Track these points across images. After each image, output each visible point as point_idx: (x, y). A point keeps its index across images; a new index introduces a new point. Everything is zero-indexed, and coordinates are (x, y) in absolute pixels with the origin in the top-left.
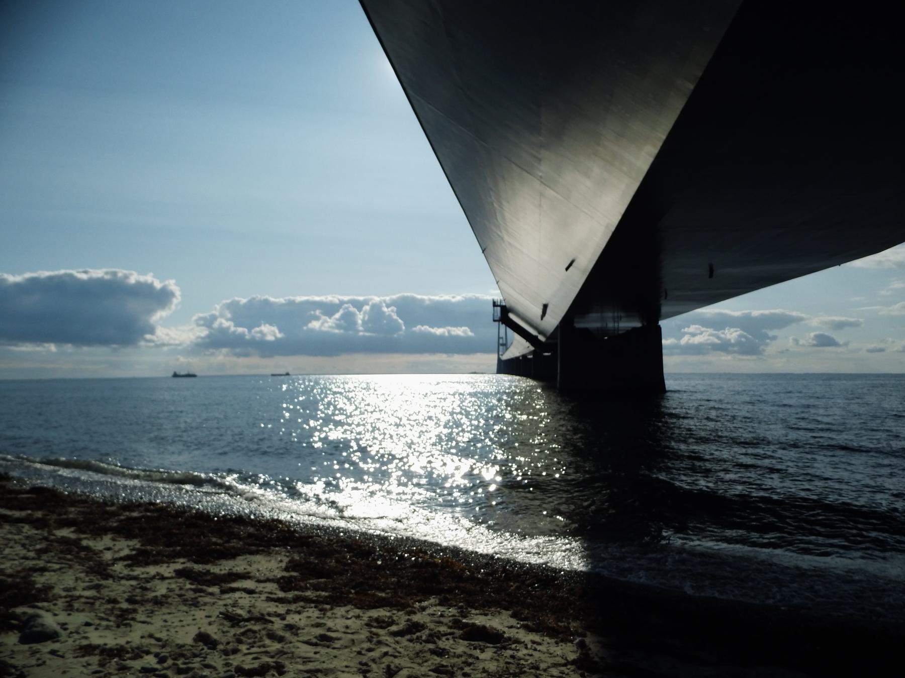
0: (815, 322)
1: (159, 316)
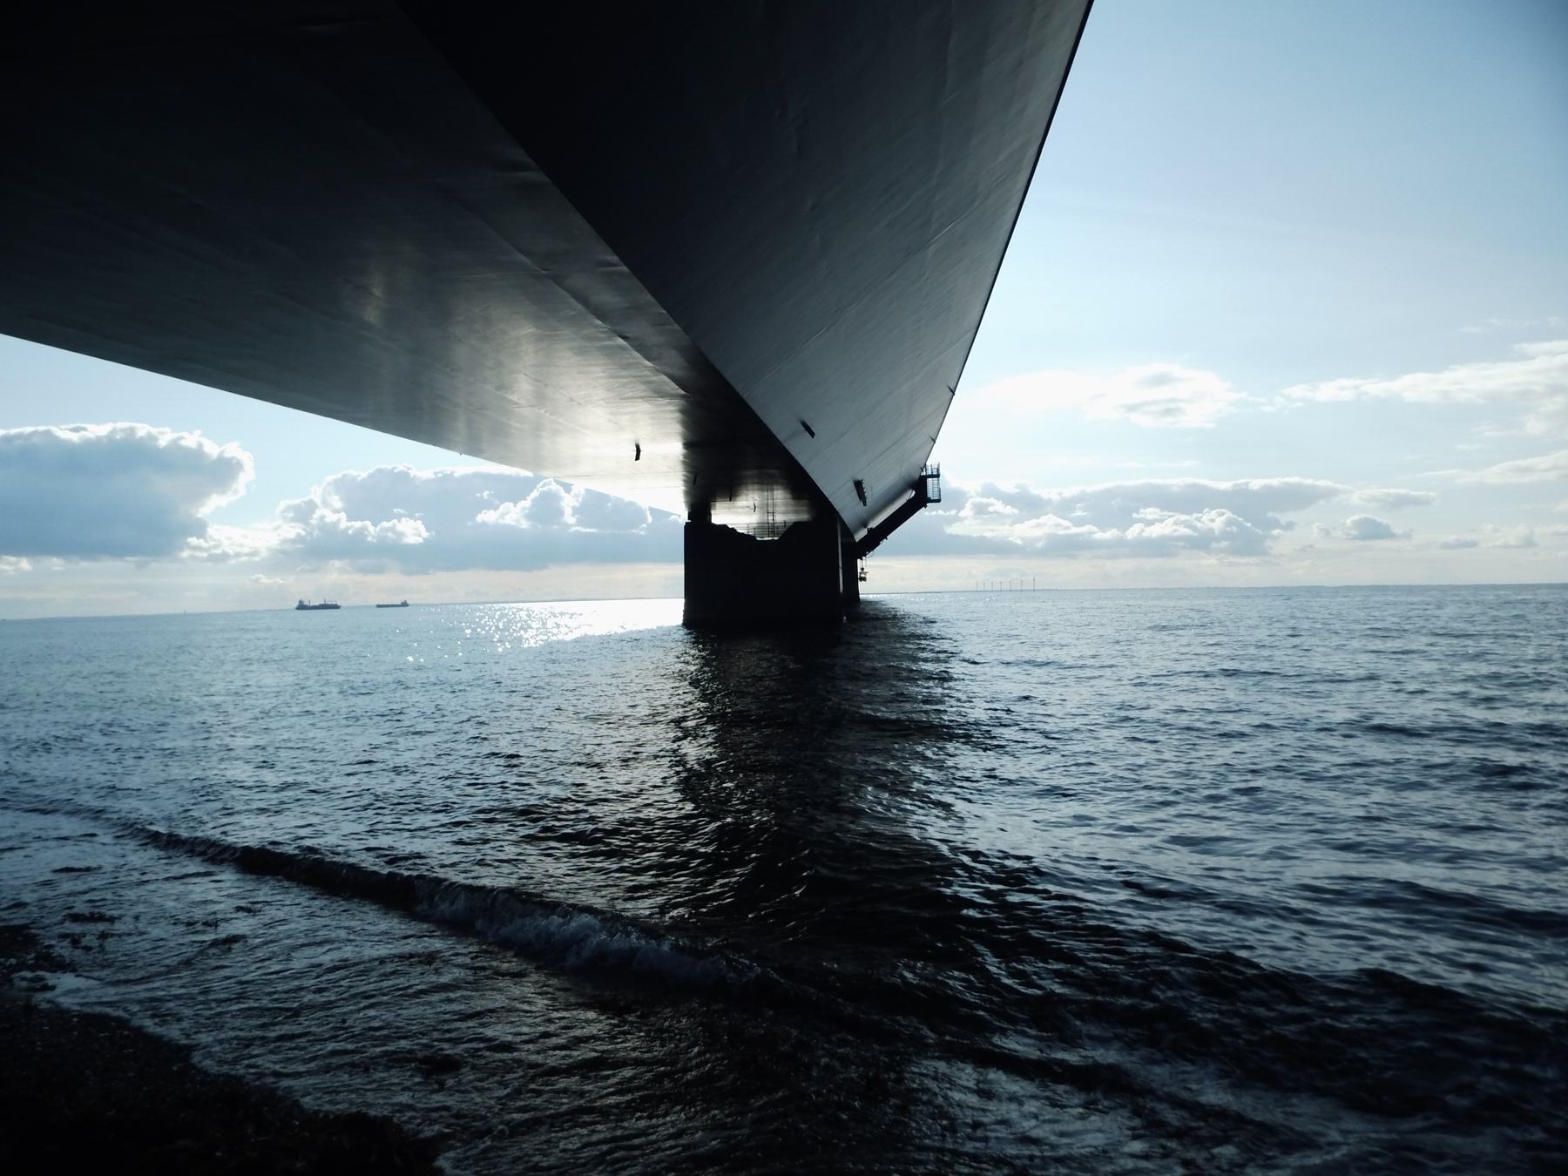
0: (1355, 498)
1: (210, 507)
